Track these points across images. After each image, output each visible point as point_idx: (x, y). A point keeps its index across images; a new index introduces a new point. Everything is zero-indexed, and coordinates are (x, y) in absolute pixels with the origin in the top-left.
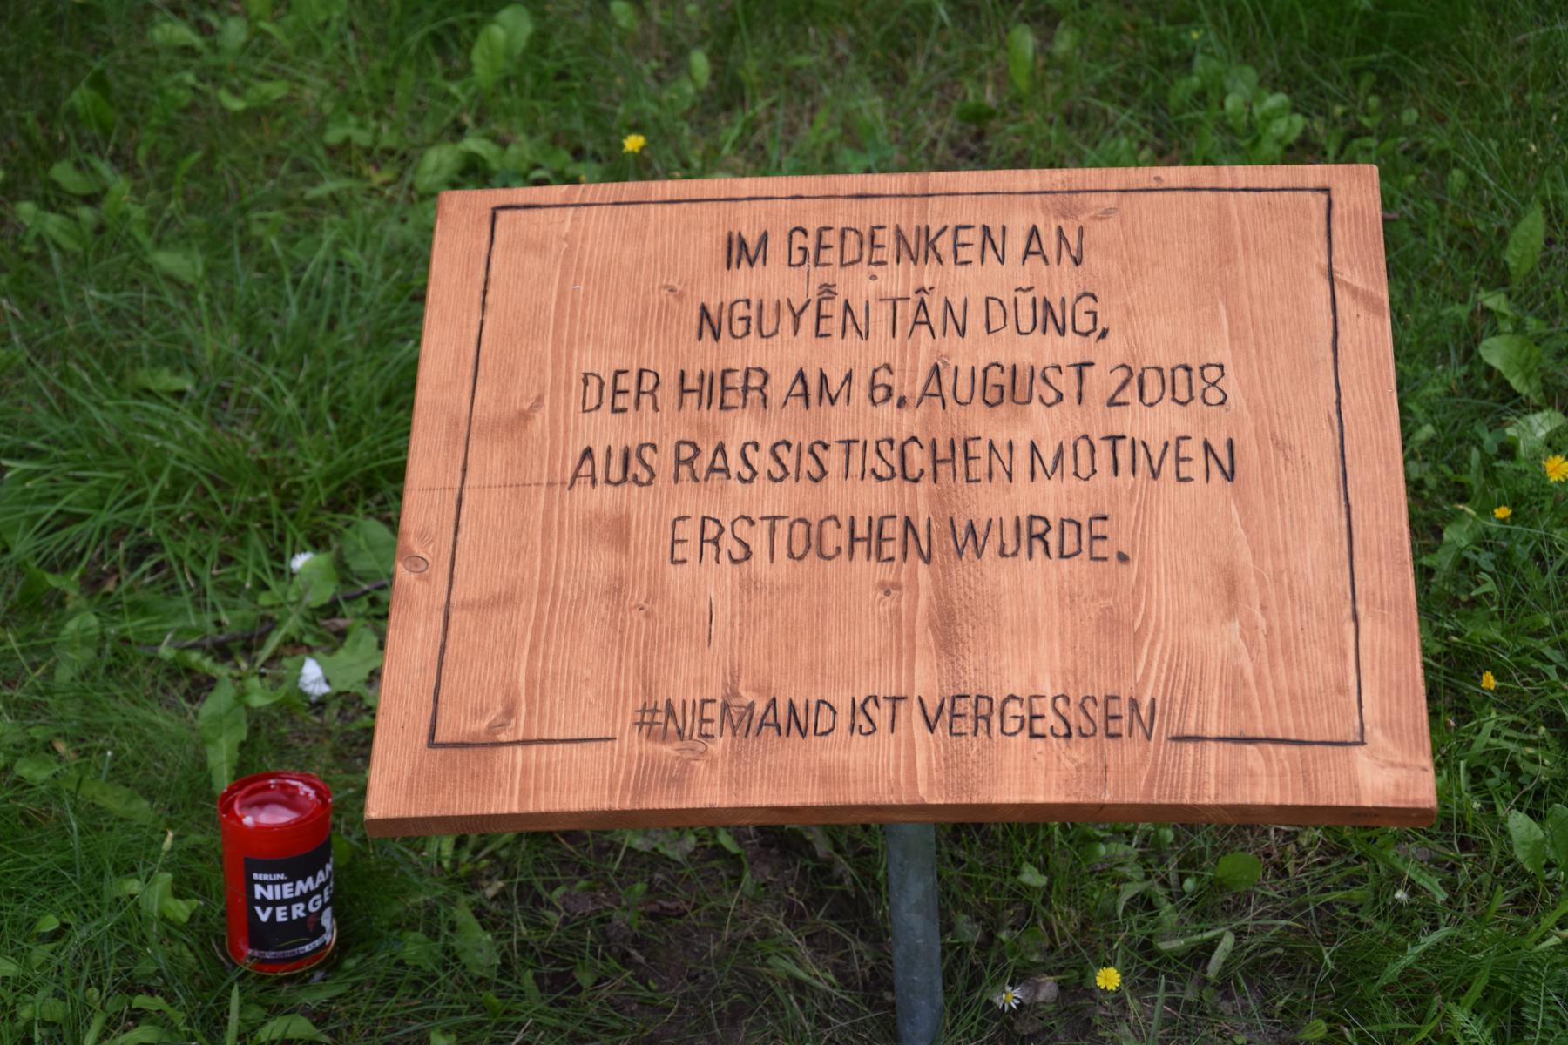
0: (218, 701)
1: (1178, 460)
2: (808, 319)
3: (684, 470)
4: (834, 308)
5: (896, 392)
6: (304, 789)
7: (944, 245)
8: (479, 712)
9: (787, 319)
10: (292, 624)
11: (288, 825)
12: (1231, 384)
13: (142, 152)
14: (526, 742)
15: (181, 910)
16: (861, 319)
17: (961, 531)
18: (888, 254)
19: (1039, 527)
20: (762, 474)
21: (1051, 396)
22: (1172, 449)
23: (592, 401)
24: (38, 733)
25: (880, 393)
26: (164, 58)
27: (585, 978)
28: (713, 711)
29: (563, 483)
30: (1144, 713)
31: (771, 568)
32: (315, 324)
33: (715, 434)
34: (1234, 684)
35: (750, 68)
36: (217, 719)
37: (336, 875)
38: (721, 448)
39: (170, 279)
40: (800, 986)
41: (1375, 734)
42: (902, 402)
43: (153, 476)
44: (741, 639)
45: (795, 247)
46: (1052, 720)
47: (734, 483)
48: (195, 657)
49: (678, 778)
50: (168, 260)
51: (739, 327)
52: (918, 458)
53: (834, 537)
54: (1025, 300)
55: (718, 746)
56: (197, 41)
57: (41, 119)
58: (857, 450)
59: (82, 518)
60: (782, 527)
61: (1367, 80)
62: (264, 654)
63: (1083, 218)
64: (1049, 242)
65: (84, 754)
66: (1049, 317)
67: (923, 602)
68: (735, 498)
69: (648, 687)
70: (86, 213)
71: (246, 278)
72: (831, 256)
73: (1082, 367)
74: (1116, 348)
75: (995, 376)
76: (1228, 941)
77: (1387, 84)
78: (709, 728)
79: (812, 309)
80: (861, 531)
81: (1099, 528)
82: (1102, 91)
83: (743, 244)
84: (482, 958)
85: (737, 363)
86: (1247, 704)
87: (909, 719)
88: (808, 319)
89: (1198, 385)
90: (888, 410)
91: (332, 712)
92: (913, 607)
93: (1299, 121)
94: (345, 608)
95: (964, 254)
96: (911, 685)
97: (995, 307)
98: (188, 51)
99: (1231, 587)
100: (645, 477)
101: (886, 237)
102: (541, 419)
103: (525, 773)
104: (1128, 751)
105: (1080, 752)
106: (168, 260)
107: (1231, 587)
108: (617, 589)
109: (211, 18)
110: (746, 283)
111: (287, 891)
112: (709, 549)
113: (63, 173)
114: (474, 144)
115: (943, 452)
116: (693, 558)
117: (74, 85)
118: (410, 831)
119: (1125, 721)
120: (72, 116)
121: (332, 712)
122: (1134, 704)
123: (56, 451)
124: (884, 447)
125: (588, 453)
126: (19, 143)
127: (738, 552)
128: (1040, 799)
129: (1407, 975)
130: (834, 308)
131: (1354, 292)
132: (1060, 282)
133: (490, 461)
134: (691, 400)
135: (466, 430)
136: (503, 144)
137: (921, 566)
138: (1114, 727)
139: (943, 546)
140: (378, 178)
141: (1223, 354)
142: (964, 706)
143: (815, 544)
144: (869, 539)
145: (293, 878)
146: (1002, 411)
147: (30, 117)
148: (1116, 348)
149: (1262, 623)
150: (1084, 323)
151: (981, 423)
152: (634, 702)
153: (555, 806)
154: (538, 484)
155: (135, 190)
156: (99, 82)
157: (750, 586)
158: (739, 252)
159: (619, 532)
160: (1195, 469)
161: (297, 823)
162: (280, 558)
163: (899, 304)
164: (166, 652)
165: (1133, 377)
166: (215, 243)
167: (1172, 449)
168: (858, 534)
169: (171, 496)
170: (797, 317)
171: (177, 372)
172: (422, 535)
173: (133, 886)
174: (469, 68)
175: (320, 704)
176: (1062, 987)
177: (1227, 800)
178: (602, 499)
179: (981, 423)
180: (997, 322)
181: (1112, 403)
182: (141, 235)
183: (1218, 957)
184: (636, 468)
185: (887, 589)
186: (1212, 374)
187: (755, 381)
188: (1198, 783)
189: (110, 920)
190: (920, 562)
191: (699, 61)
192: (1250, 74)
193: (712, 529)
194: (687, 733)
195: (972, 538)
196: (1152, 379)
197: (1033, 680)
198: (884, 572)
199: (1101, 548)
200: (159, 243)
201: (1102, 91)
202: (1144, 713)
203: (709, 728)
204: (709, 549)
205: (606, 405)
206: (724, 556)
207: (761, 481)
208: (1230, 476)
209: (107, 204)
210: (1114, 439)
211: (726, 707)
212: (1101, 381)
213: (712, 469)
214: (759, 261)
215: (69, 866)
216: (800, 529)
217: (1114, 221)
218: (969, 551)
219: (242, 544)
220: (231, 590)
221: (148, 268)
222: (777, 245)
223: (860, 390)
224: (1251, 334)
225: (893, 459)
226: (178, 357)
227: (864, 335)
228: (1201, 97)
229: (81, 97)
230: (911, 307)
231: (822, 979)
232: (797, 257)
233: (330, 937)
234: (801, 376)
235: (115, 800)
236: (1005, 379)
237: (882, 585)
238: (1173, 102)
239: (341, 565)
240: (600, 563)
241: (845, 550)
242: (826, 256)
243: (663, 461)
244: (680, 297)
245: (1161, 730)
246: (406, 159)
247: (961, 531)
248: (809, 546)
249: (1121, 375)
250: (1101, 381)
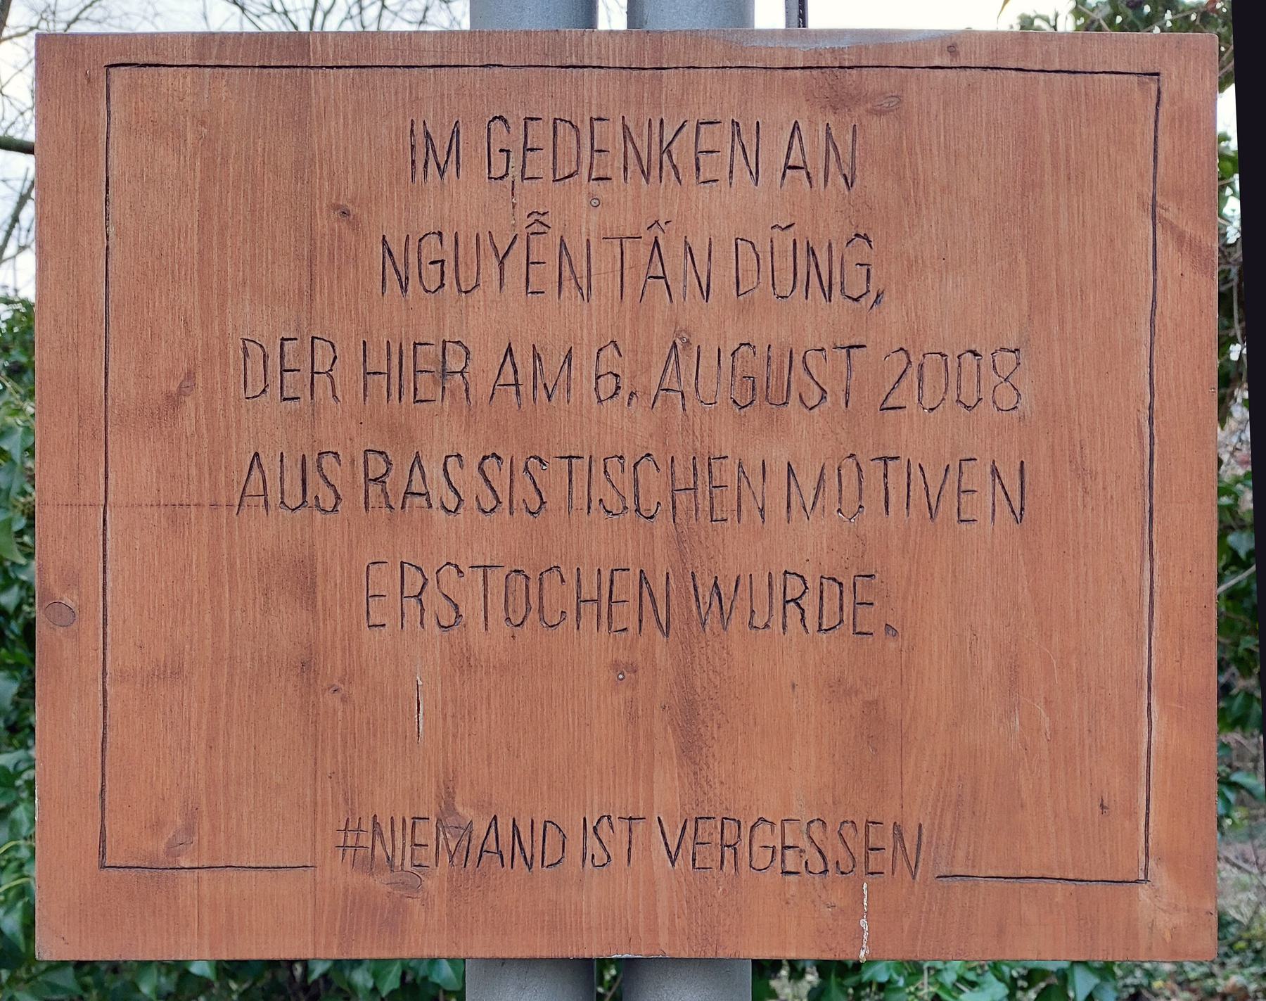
2: (516, 262)
3: (375, 489)
5: (625, 384)
7: (683, 152)
8: (157, 826)
16: (581, 269)
17: (705, 592)
19: (795, 587)
20: (469, 502)
22: (954, 475)
23: (256, 387)
28: (427, 832)
29: (229, 505)
30: (910, 846)
33: (412, 440)
44: (455, 736)
45: (495, 149)
53: (558, 596)
54: (784, 241)
72: (540, 164)
79: (520, 245)
80: (589, 591)
87: (648, 848)
88: (516, 262)
96: (650, 805)
119: (888, 853)
122: (898, 830)
124: (613, 464)
127: (448, 617)
130: (545, 249)
131: (1180, 238)
138: (875, 861)
144: (598, 601)
154: (198, 505)
157: (465, 662)
163: (627, 243)
167: (954, 475)
168: (585, 596)
190: (659, 633)
193: (414, 581)
194: (398, 862)
199: (868, 618)
202: (910, 846)
205: (274, 390)
206: (430, 620)
214: (452, 168)
218: (713, 621)
224: (1055, 304)
225: (625, 481)
227: (583, 292)
237: (615, 666)
241: (571, 616)
247: (705, 592)
248: (528, 609)
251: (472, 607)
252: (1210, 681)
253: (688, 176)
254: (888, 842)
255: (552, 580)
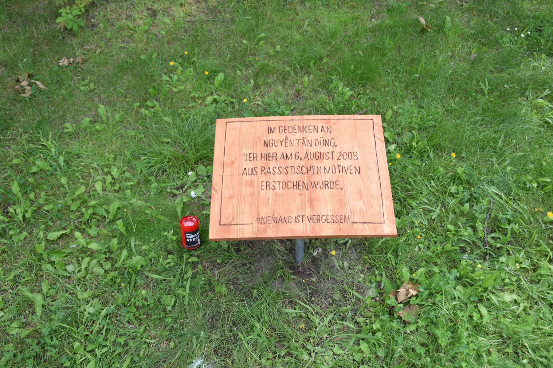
0: (178, 199)
1: (350, 170)
2: (283, 143)
3: (263, 172)
4: (288, 141)
6: (194, 219)
7: (307, 129)
8: (228, 219)
9: (280, 143)
10: (189, 184)
11: (191, 226)
12: (358, 156)
13: (161, 99)
14: (237, 224)
15: (174, 238)
17: (313, 184)
18: (297, 131)
19: (327, 183)
21: (327, 158)
23: (245, 159)
24: (149, 204)
25: (297, 157)
26: (164, 82)
27: (242, 249)
28: (270, 218)
30: (347, 218)
31: (279, 191)
32: (190, 130)
34: (362, 212)
35: (260, 83)
36: (178, 203)
37: (200, 233)
38: (269, 168)
39: (166, 122)
40: (278, 250)
41: (386, 221)
42: (301, 159)
43: (165, 158)
46: (331, 219)
47: (272, 174)
48: (173, 190)
49: (264, 231)
50: (165, 119)
51: (271, 145)
52: (304, 170)
53: (290, 185)
54: (322, 140)
55: (271, 225)
56: (169, 79)
57: (145, 94)
58: (293, 168)
59: (154, 166)
60: (281, 183)
61: (361, 85)
62: (184, 189)
63: (331, 124)
64: (325, 129)
65: (156, 208)
66: (326, 143)
67: (307, 197)
68: (272, 178)
69: (258, 214)
70: (152, 110)
71: (178, 122)
72: (286, 131)
73: (332, 152)
74: (338, 149)
75: (317, 154)
76: (350, 241)
77: (364, 86)
78: (269, 222)
80: (295, 184)
81: (337, 183)
82: (319, 86)
83: (271, 129)
84: (225, 246)
85: (271, 152)
86: (365, 216)
88: (283, 143)
89: (353, 156)
90: (299, 161)
91: (196, 200)
92: (305, 198)
93: (351, 92)
94: (198, 181)
95: (311, 131)
97: (316, 141)
98: (168, 81)
99: (361, 194)
100: (256, 173)
101: (296, 128)
102: (237, 162)
103: (237, 230)
104: (344, 225)
105: (336, 226)
106: (165, 119)
107: (361, 194)
108: (252, 195)
109: (171, 75)
110: (272, 136)
111: (192, 237)
112: (268, 187)
113: (149, 103)
114: (215, 97)
115: (309, 168)
116: (265, 189)
117: (150, 88)
118: (216, 241)
120: (150, 93)
121: (196, 200)
122: (345, 217)
123: (149, 154)
125: (245, 169)
126: (141, 98)
127: (273, 188)
128: (329, 235)
129: (380, 246)
130: (288, 141)
131: (378, 138)
132: (328, 137)
133: (228, 171)
134: (263, 159)
135: (223, 165)
136: (220, 96)
137: (306, 191)
138: (342, 221)
139: (310, 187)
140: (199, 102)
141: (356, 150)
142: (315, 217)
143: (287, 186)
145: (193, 234)
146: (319, 161)
147: (143, 94)
148: (338, 149)
149: (366, 201)
150: (332, 144)
151: (315, 163)
152: (256, 217)
153: (243, 237)
155: (160, 105)
156: (154, 87)
157: (275, 194)
158: (271, 130)
159: (251, 184)
160: (353, 172)
161: (193, 225)
162: (186, 172)
164: (169, 190)
165: (342, 154)
166: (173, 115)
169: (168, 162)
170: (281, 143)
171: (168, 138)
172: (216, 185)
173: (166, 233)
174: (214, 83)
175: (195, 198)
176: (323, 249)
177: (362, 234)
178: (248, 178)
179: (315, 163)
180: (317, 144)
181: (338, 159)
182: (161, 114)
183: (348, 244)
184: (254, 172)
185: (300, 195)
186: (355, 154)
187: (274, 155)
188: (357, 231)
189: (162, 239)
191: (252, 81)
192: (342, 84)
193: (268, 184)
195: (315, 185)
196: (345, 155)
197: (327, 212)
198: (300, 192)
199: (338, 187)
200: (165, 116)
201: (319, 86)
202: (347, 218)
203: (269, 222)
204: (268, 187)
207: (277, 174)
208: (359, 173)
209: (155, 108)
210: (339, 166)
211: (272, 218)
212: (336, 155)
213: (268, 172)
215: (155, 230)
216: (284, 183)
217: (336, 125)
218: (314, 187)
219: (180, 170)
220: (178, 178)
221: (162, 120)
222: (277, 129)
223: (293, 157)
225: (300, 170)
226: (168, 136)
228: (335, 87)
229: (151, 90)
230: (302, 141)
231: (283, 249)
232: (281, 131)
233: (199, 243)
234: (283, 154)
235: (162, 218)
236: (319, 155)
238: (330, 88)
239: (197, 173)
240: (248, 190)
242: (286, 131)
243: (259, 170)
244: (260, 139)
245: (350, 221)
246: (204, 99)
247: (313, 184)
249: (339, 154)
250: (336, 155)
251: (277, 186)
252: (391, 195)
253: (308, 132)
254: (343, 218)
255: (289, 183)
